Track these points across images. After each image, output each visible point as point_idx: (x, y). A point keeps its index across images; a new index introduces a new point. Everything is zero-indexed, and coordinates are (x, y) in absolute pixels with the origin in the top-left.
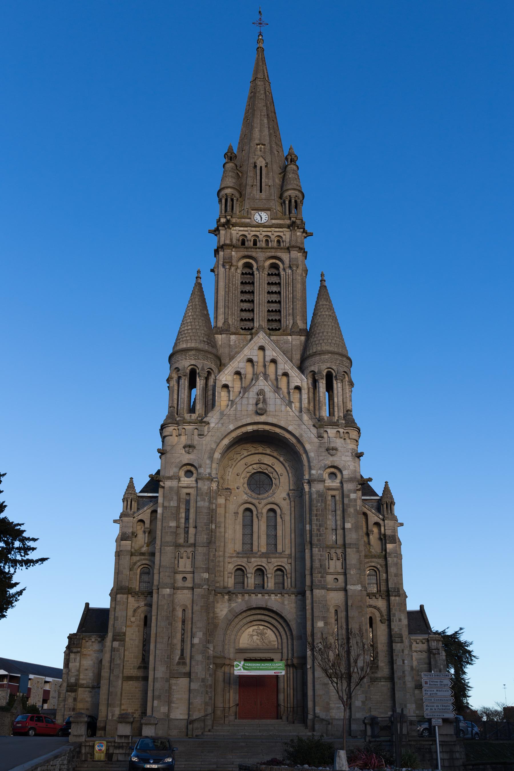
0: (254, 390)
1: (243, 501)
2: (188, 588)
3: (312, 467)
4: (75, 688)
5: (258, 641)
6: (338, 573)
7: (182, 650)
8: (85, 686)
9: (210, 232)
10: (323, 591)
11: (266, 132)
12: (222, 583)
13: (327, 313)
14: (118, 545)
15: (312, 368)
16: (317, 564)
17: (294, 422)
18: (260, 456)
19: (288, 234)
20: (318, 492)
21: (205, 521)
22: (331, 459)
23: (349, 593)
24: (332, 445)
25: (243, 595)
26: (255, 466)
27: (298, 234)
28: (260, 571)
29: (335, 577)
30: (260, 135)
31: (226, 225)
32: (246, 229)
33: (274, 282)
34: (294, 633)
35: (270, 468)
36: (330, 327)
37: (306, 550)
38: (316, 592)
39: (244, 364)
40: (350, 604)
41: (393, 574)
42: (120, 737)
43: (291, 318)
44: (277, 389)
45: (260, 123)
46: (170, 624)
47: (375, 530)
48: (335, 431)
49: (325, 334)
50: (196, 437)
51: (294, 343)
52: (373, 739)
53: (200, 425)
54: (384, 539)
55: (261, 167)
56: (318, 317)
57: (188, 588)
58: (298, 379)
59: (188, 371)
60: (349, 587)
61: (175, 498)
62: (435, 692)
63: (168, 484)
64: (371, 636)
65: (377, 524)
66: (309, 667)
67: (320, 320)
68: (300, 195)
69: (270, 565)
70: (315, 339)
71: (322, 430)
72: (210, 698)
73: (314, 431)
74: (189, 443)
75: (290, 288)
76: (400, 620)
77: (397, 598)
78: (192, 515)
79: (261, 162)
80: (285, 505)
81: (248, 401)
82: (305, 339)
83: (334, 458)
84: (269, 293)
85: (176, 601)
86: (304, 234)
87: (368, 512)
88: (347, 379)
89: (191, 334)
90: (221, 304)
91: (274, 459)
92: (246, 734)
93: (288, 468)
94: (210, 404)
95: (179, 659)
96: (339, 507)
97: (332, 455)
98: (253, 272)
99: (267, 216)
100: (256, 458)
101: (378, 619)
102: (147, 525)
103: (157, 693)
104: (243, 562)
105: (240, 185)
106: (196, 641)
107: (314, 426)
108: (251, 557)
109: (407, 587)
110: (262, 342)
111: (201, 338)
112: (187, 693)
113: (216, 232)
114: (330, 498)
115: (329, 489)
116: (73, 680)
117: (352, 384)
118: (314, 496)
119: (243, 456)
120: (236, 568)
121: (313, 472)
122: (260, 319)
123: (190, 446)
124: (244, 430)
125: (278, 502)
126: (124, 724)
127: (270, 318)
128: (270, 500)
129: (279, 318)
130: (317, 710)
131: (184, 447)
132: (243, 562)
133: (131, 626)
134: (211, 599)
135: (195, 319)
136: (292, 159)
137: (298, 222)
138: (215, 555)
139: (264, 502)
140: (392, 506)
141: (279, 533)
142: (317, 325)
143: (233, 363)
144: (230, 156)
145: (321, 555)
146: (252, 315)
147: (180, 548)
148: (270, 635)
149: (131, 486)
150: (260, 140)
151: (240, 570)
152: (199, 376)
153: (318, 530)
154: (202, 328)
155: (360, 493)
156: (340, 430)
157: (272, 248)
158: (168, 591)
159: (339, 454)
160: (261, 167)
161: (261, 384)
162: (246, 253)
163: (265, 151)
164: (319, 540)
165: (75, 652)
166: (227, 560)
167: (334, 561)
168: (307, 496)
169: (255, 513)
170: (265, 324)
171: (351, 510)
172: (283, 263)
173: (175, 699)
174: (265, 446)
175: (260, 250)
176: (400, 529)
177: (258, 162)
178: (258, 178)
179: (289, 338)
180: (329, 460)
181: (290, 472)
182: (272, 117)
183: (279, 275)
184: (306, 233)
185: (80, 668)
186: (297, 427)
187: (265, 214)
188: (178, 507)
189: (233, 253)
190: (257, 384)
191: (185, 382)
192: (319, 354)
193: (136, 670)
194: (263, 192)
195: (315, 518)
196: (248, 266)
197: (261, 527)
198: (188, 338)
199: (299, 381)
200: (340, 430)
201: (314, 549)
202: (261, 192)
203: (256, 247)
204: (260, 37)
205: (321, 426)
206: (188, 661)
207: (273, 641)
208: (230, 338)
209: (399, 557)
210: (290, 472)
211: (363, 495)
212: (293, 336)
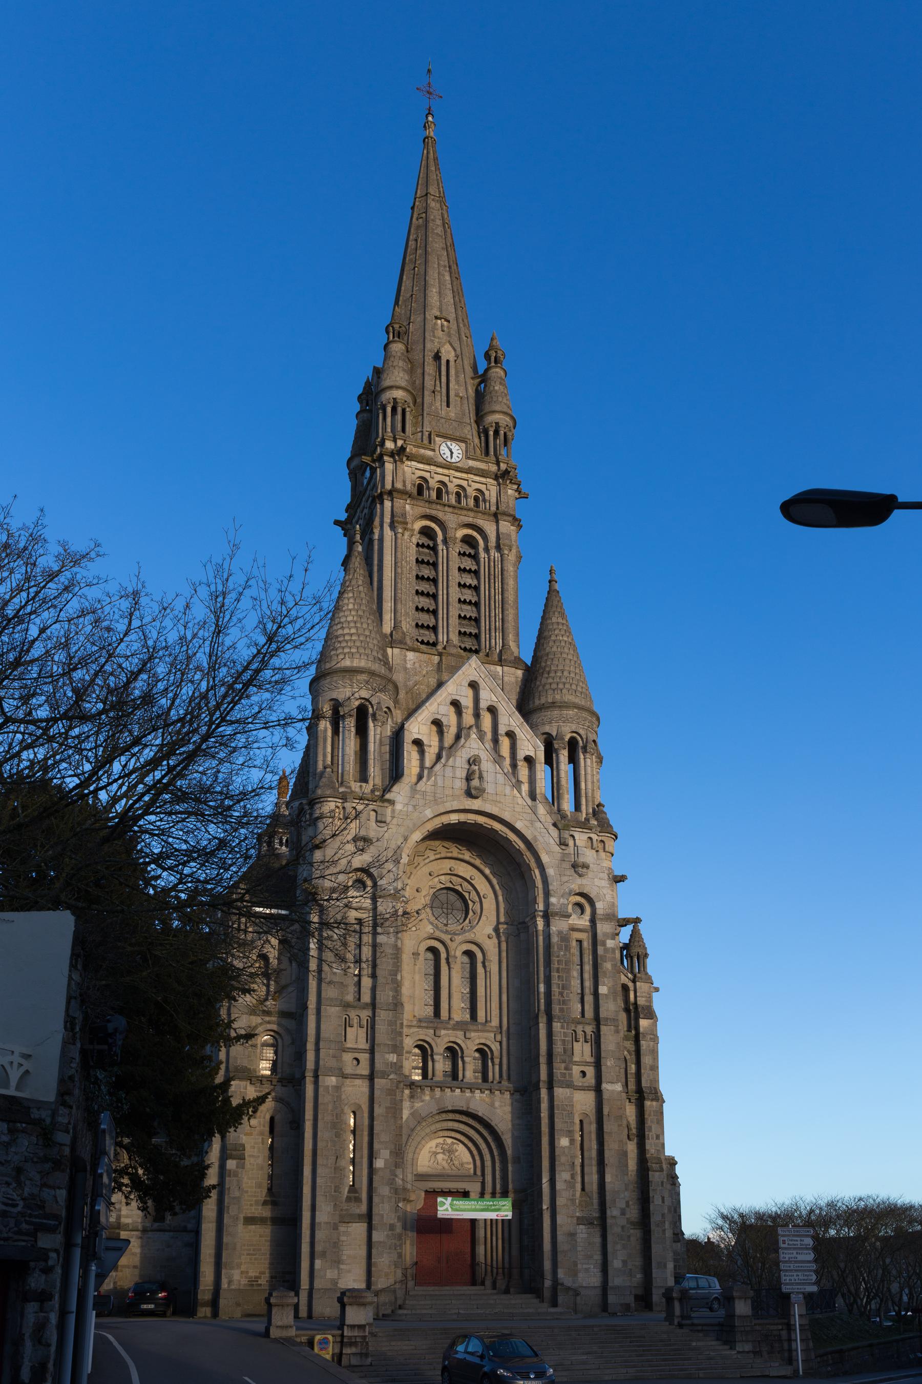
1: (426, 935)
2: (361, 1077)
3: (552, 892)
4: (117, 1231)
5: (446, 1165)
6: (587, 1064)
8: (131, 1227)
10: (568, 1090)
11: (449, 298)
13: (565, 639)
16: (558, 1048)
17: (525, 815)
18: (452, 863)
19: (494, 490)
20: (560, 933)
21: (390, 968)
22: (579, 881)
23: (605, 1096)
24: (581, 860)
25: (432, 1090)
26: (442, 878)
27: (510, 492)
28: (453, 1053)
29: (583, 1068)
30: (440, 301)
31: (398, 455)
32: (427, 467)
33: (468, 568)
34: (509, 1152)
35: (466, 884)
36: (573, 663)
37: (541, 1025)
39: (446, 708)
40: (606, 1111)
41: (648, 1067)
42: (352, 1327)
43: (499, 635)
46: (338, 1135)
48: (584, 837)
49: (566, 673)
51: (506, 679)
53: (381, 804)
55: (448, 361)
56: (551, 644)
57: (361, 1077)
60: (605, 1086)
62: (795, 1255)
64: (352, 1121)
66: (545, 1207)
67: (554, 649)
68: (511, 424)
70: (550, 680)
71: (566, 834)
73: (554, 832)
75: (498, 585)
77: (654, 1103)
79: (448, 353)
80: (491, 946)
81: (454, 773)
82: (523, 674)
83: (584, 881)
85: (343, 1097)
89: (358, 644)
91: (474, 870)
92: (461, 1311)
93: (497, 887)
95: (349, 1192)
96: (588, 958)
97: (580, 876)
98: (436, 545)
99: (460, 451)
100: (447, 865)
104: (427, 1034)
107: (555, 825)
108: (440, 1028)
109: (664, 1087)
110: (474, 676)
111: (375, 653)
114: (574, 943)
115: (573, 929)
118: (555, 939)
120: (421, 1043)
124: (445, 819)
125: (480, 941)
126: (355, 1307)
127: (463, 630)
128: (470, 936)
129: (477, 631)
130: (561, 1274)
132: (427, 1034)
133: (251, 1134)
135: (361, 617)
139: (458, 939)
142: (551, 656)
143: (430, 705)
145: (565, 1034)
146: (433, 620)
147: (349, 1009)
148: (463, 1154)
150: (441, 311)
153: (561, 994)
154: (373, 635)
156: (592, 835)
159: (590, 874)
160: (448, 361)
161: (473, 746)
162: (428, 511)
163: (449, 332)
164: (561, 1010)
166: (405, 1031)
167: (580, 1044)
168: (541, 938)
173: (344, 1257)
174: (463, 846)
175: (450, 510)
176: (655, 995)
177: (443, 350)
180: (576, 884)
181: (499, 893)
184: (520, 493)
186: (529, 825)
187: (457, 447)
189: (407, 506)
190: (467, 744)
192: (560, 707)
193: (260, 1207)
194: (451, 406)
196: (426, 532)
197: (455, 981)
198: (354, 650)
199: (531, 748)
200: (592, 835)
201: (554, 1024)
202: (448, 406)
203: (421, 498)
204: (430, 118)
205: (567, 827)
207: (468, 1163)
208: (406, 656)
209: (655, 1039)
210: (499, 893)
212: (505, 668)
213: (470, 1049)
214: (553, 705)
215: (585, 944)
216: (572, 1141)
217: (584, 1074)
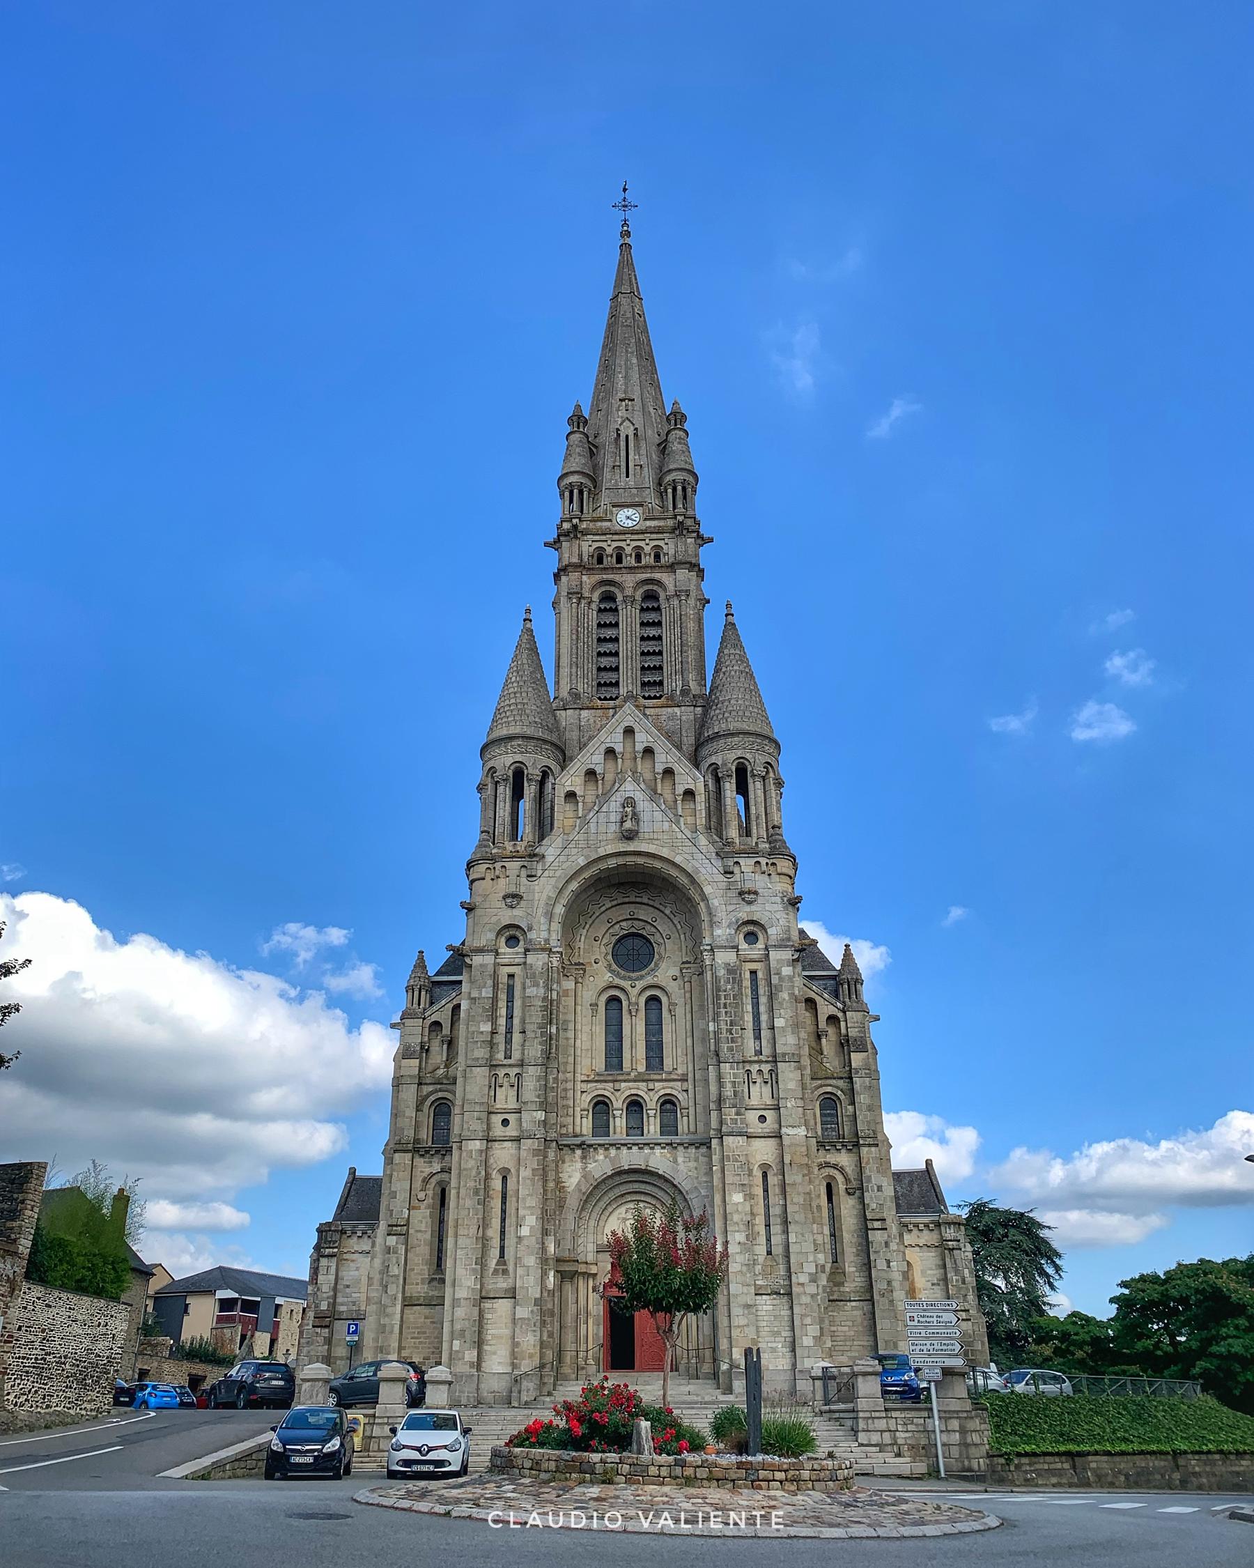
0: (618, 798)
7: (502, 1248)
9: (546, 544)
12: (571, 1127)
14: (398, 1067)
15: (713, 759)
22: (748, 908)
23: (786, 1141)
24: (748, 886)
26: (624, 924)
28: (635, 1105)
38: (728, 1140)
40: (787, 1160)
44: (654, 794)
45: (628, 361)
47: (831, 1031)
50: (524, 880)
52: (827, 1408)
54: (845, 1044)
58: (689, 778)
59: (510, 773)
60: (784, 1130)
61: (490, 982)
63: (477, 960)
65: (832, 1019)
69: (651, 1093)
71: (730, 862)
72: (551, 1335)
73: (718, 863)
74: (512, 889)
75: (678, 630)
76: (880, 1188)
78: (517, 1012)
84: (643, 639)
86: (700, 541)
87: (817, 999)
88: (771, 775)
90: (565, 661)
94: (544, 827)
100: (625, 912)
101: (842, 1187)
102: (446, 1030)
103: (458, 1327)
104: (606, 1090)
105: (595, 467)
106: (525, 1231)
110: (628, 722)
112: (510, 1325)
113: (556, 544)
116: (324, 1306)
117: (779, 784)
119: (603, 909)
121: (718, 932)
122: (628, 682)
123: (514, 896)
124: (603, 866)
125: (663, 984)
131: (505, 897)
133: (419, 1208)
134: (551, 1155)
136: (677, 418)
137: (689, 522)
138: (556, 1079)
139: (640, 984)
140: (859, 986)
141: (667, 1037)
144: (578, 420)
145: (735, 1076)
149: (421, 964)
150: (625, 392)
151: (601, 1106)
152: (529, 780)
155: (799, 967)
157: (646, 567)
158: (476, 1145)
159: (760, 900)
161: (630, 788)
165: (328, 1256)
166: (579, 1086)
169: (625, 1003)
170: (637, 690)
171: (785, 995)
172: (665, 590)
173: (489, 1337)
176: (873, 1026)
177: (622, 428)
178: (623, 453)
179: (676, 709)
180: (745, 912)
182: (647, 358)
183: (658, 609)
185: (336, 1283)
188: (495, 999)
191: (505, 792)
195: (723, 1011)
197: (635, 1029)
199: (690, 780)
206: (511, 1268)
211: (804, 970)
213: (651, 1103)
214: (717, 736)
215: (760, 975)
216: (750, 1197)
217: (762, 1119)
